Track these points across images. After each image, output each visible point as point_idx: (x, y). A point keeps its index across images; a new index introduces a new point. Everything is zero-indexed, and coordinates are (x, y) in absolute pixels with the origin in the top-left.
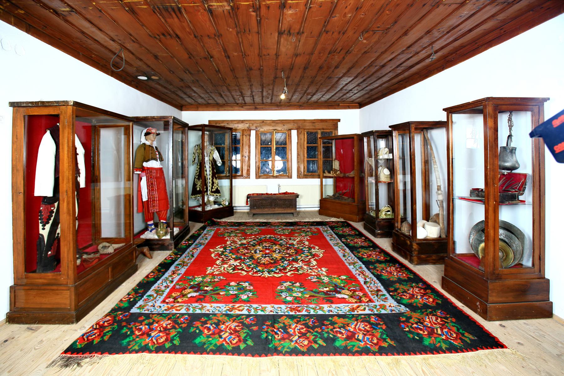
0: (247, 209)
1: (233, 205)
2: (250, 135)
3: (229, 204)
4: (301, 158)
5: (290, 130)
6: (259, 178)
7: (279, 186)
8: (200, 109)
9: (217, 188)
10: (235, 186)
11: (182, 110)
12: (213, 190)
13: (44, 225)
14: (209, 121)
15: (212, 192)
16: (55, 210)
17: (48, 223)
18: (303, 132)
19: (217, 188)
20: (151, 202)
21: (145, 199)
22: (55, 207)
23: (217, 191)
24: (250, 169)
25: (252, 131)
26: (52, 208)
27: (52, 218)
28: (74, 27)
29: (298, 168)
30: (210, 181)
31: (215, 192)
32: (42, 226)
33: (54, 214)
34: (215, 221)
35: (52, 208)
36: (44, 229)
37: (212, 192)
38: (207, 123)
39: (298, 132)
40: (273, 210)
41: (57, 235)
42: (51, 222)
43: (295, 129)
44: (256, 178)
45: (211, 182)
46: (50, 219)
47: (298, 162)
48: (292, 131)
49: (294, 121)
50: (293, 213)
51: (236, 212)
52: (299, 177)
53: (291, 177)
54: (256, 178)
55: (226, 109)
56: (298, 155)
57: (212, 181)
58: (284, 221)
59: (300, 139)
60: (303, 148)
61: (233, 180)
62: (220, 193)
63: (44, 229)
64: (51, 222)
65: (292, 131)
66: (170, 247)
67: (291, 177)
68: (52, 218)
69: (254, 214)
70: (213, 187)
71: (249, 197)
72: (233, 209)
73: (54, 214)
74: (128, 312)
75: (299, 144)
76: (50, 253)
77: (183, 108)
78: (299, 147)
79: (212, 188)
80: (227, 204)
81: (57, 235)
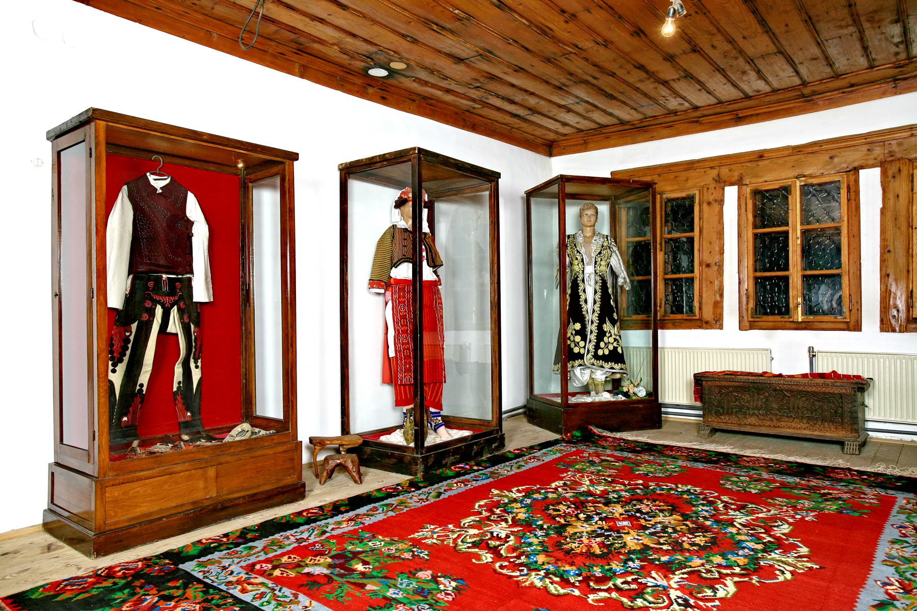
0: (693, 417)
1: (660, 401)
2: (721, 202)
3: (648, 394)
4: (896, 261)
5: (856, 170)
6: (751, 328)
7: (812, 353)
8: (590, 145)
9: (615, 348)
10: (663, 348)
11: (551, 155)
12: (600, 352)
13: (115, 365)
14: (612, 173)
15: (596, 356)
16: (132, 338)
17: (121, 361)
18: (904, 172)
19: (615, 348)
20: (401, 359)
21: (115, 300)
22: (131, 332)
23: (616, 357)
24: (722, 301)
25: (727, 189)
26: (128, 334)
27: (128, 353)
28: (779, 92)
29: (886, 296)
30: (594, 328)
31: (605, 358)
32: (112, 365)
33: (130, 346)
34: (594, 434)
35: (128, 334)
36: (114, 371)
37: (596, 356)
38: (609, 176)
39: (884, 174)
40: (775, 423)
41: (138, 388)
42: (126, 359)
43: (873, 166)
44: (741, 328)
45: (595, 331)
46: (125, 355)
47: (884, 276)
48: (862, 173)
49: (869, 139)
50: (841, 443)
51: (666, 421)
52: (886, 326)
53: (857, 327)
54: (741, 328)
55: (654, 134)
56: (885, 251)
57: (600, 327)
58: (791, 459)
59: (891, 196)
60: (904, 227)
61: (660, 331)
62: (623, 362)
63: (114, 371)
64: (126, 359)
65: (862, 173)
66: (414, 468)
67: (857, 327)
68: (128, 353)
69: (714, 431)
70: (602, 345)
71: (700, 380)
72: (660, 413)
73: (130, 346)
74: (176, 564)
75: (889, 215)
76: (125, 419)
77: (555, 151)
78: (890, 225)
79: (597, 347)
80: (642, 393)
81: (138, 388)
